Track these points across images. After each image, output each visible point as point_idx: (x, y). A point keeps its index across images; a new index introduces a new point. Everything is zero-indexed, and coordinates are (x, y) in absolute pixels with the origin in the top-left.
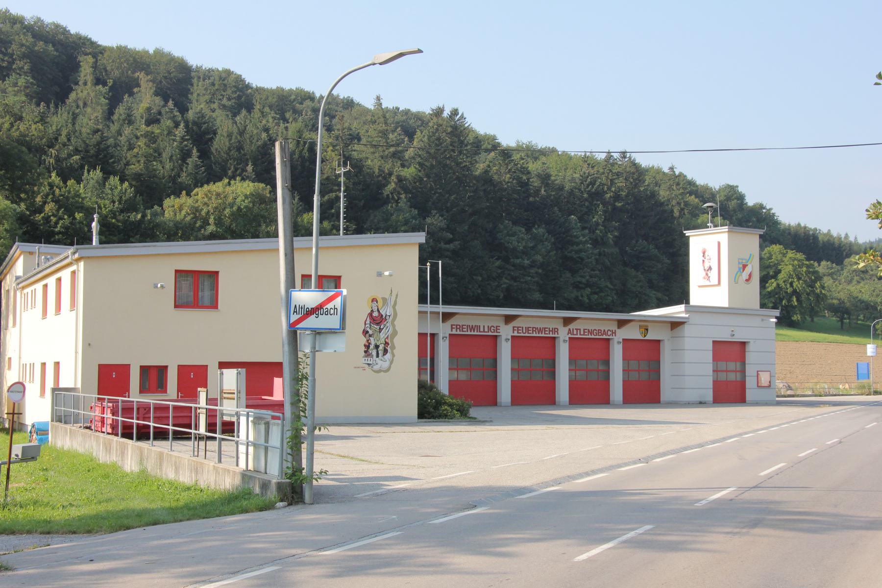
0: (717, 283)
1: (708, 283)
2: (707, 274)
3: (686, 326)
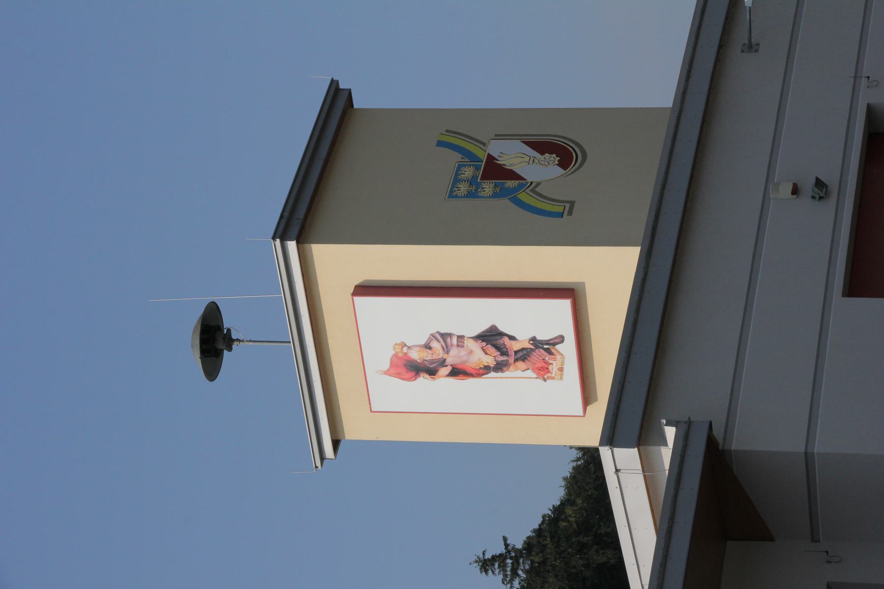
0: (565, 305)
1: (568, 350)
2: (523, 355)
3: (745, 439)
